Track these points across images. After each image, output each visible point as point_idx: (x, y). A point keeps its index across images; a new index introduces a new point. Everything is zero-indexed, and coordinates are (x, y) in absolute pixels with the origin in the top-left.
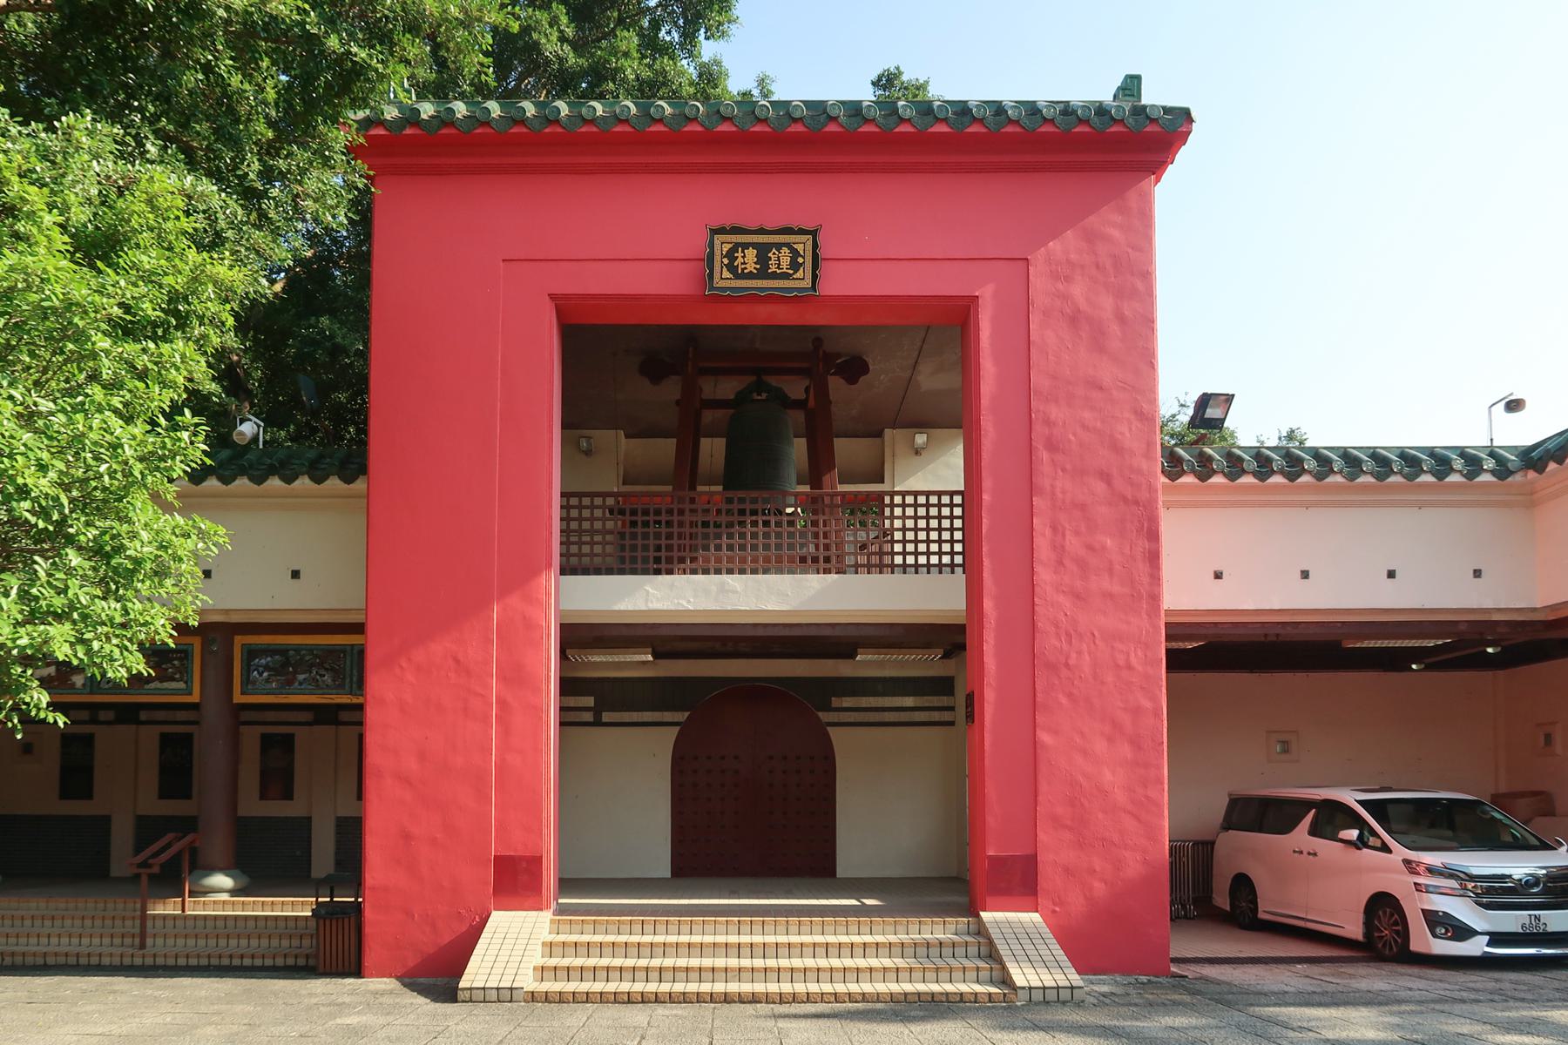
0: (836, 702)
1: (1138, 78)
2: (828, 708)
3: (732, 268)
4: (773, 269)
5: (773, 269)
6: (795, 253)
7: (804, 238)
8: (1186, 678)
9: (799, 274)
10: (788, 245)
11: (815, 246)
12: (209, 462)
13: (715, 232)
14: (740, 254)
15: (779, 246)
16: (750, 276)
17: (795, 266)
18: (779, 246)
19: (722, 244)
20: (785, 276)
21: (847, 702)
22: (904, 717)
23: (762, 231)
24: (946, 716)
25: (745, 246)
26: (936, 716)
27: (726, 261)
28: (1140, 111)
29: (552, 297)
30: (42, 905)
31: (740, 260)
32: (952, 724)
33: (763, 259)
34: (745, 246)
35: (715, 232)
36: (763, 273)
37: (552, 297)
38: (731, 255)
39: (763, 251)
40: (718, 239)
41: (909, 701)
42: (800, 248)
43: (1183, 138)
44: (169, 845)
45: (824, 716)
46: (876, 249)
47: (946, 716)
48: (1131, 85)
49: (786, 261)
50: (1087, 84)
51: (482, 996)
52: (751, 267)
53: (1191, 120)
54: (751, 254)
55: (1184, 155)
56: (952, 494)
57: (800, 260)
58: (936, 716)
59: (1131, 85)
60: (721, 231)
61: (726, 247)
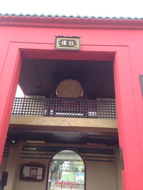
1: (19, 48)
8: (3, 157)
9: (76, 46)
10: (74, 41)
12: (66, 44)
13: (57, 37)
14: (63, 42)
15: (72, 41)
16: (65, 46)
17: (75, 44)
19: (58, 40)
20: (72, 46)
23: (68, 37)
25: (64, 40)
31: (62, 43)
33: (68, 43)
34: (64, 40)
35: (57, 37)
36: (67, 46)
38: (61, 41)
39: (68, 41)
40: (58, 39)
44: (46, 128)
51: (51, 189)
54: (65, 42)
57: (76, 43)
60: (59, 37)
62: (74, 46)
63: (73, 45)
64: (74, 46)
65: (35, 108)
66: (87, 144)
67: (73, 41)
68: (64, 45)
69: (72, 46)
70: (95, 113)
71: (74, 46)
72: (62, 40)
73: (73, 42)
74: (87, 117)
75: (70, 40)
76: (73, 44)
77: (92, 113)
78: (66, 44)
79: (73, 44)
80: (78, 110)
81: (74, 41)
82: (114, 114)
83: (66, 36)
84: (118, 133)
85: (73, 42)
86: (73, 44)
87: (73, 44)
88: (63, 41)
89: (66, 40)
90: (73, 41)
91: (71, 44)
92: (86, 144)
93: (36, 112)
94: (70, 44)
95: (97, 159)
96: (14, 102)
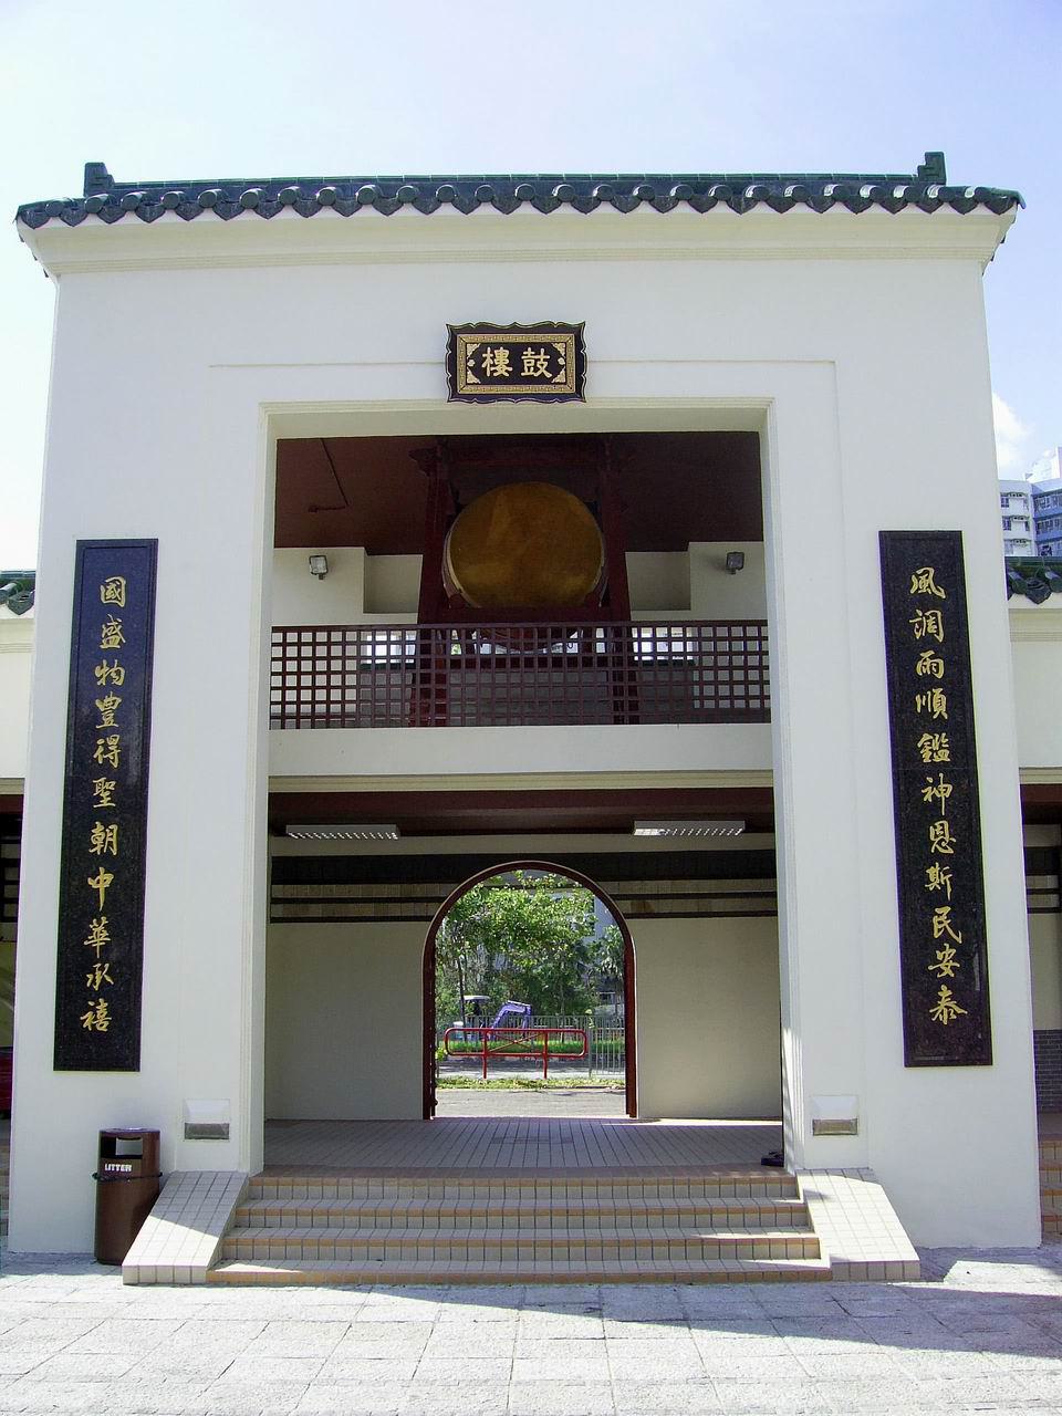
1: (260, 404)
3: (478, 371)
9: (560, 378)
12: (510, 369)
14: (488, 355)
15: (536, 347)
17: (554, 368)
20: (542, 380)
25: (495, 346)
26: (746, 905)
27: (471, 363)
31: (489, 361)
34: (495, 346)
37: (265, 405)
38: (478, 356)
39: (516, 352)
54: (502, 355)
61: (471, 349)
62: (549, 375)
63: (542, 370)
64: (549, 375)
65: (729, 701)
66: (638, 832)
67: (542, 350)
68: (495, 374)
69: (542, 380)
70: (702, 704)
71: (552, 378)
72: (484, 346)
73: (542, 357)
74: (630, 717)
75: (524, 346)
76: (546, 364)
77: (732, 704)
78: (510, 369)
79: (546, 369)
80: (753, 646)
81: (549, 349)
82: (751, 701)
83: (505, 322)
84: (1029, 872)
85: (542, 357)
86: (546, 369)
87: (546, 364)
88: (492, 352)
89: (506, 346)
90: (542, 350)
91: (536, 369)
92: (630, 830)
93: (732, 683)
94: (526, 365)
95: (691, 906)
96: (739, 709)
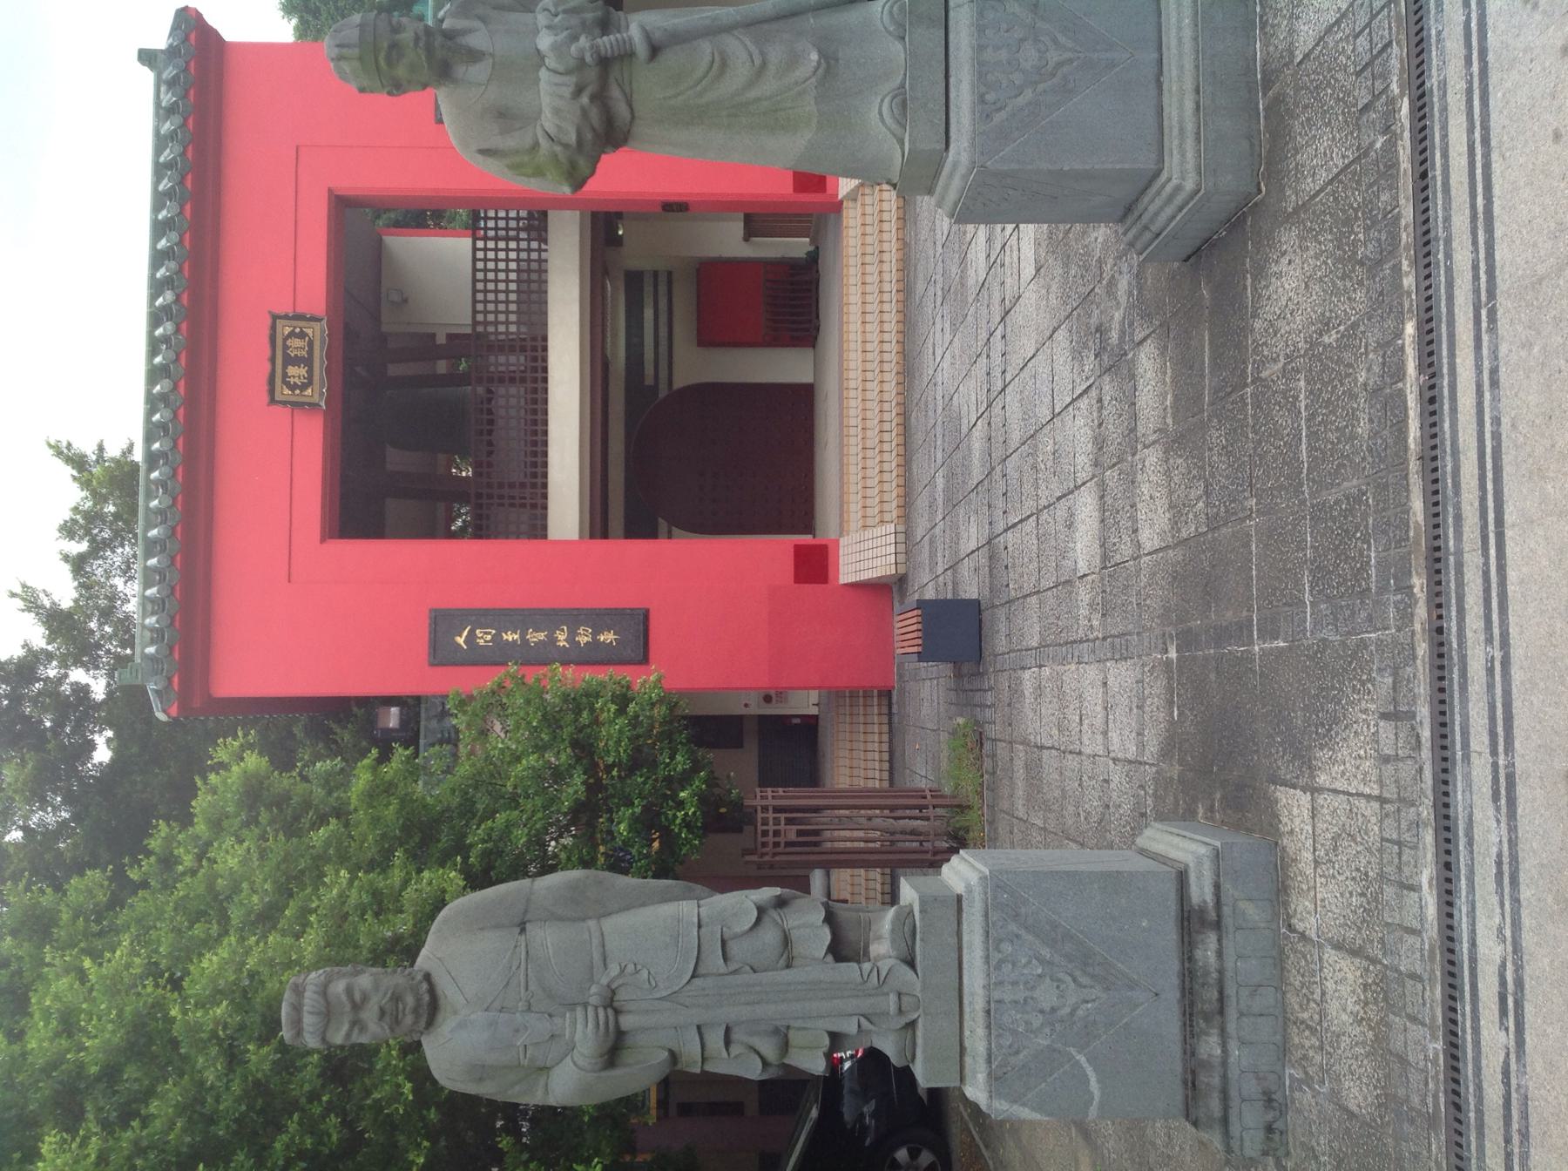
0: (649, 381)
2: (655, 387)
3: (304, 387)
4: (304, 354)
5: (304, 354)
6: (292, 334)
7: (279, 330)
9: (309, 331)
10: (285, 339)
11: (286, 317)
15: (286, 347)
17: (302, 335)
18: (286, 347)
20: (311, 344)
21: (649, 369)
22: (663, 319)
23: (273, 360)
24: (663, 279)
25: (285, 375)
26: (662, 289)
28: (172, 52)
29: (323, 540)
30: (852, 232)
32: (670, 274)
33: (296, 361)
34: (285, 375)
35: (273, 401)
36: (308, 362)
37: (323, 540)
38: (293, 387)
39: (289, 361)
41: (648, 313)
42: (288, 330)
43: (199, 16)
45: (663, 393)
46: (282, 272)
47: (663, 279)
48: (147, 57)
49: (297, 343)
50: (139, 94)
52: (303, 371)
53: (186, 9)
54: (292, 370)
55: (212, 20)
56: (475, 249)
58: (662, 289)
59: (147, 57)
60: (272, 391)
61: (286, 391)
69: (311, 344)
